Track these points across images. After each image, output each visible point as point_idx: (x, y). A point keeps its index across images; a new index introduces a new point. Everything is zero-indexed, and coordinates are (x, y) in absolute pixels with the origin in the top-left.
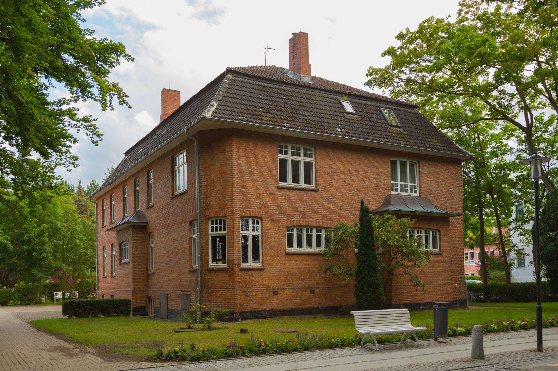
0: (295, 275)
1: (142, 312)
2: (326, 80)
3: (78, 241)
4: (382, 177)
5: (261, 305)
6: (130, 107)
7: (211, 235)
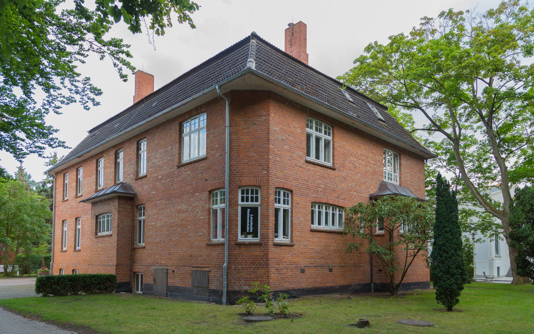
0: (317, 253)
1: (126, 287)
3: (25, 216)
5: (291, 284)
6: (193, 26)
7: (240, 205)
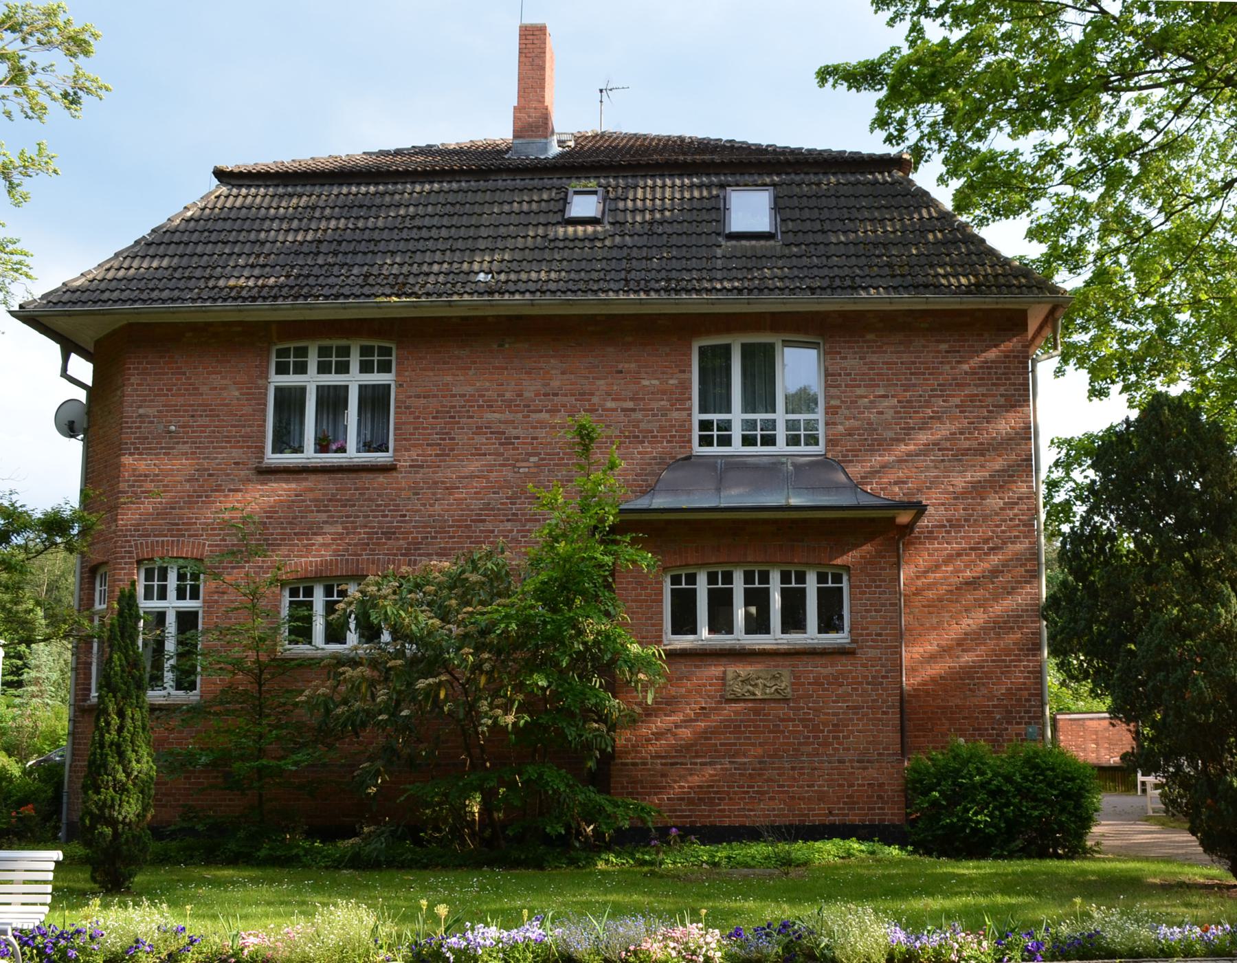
2: (682, 139)
4: (655, 405)
